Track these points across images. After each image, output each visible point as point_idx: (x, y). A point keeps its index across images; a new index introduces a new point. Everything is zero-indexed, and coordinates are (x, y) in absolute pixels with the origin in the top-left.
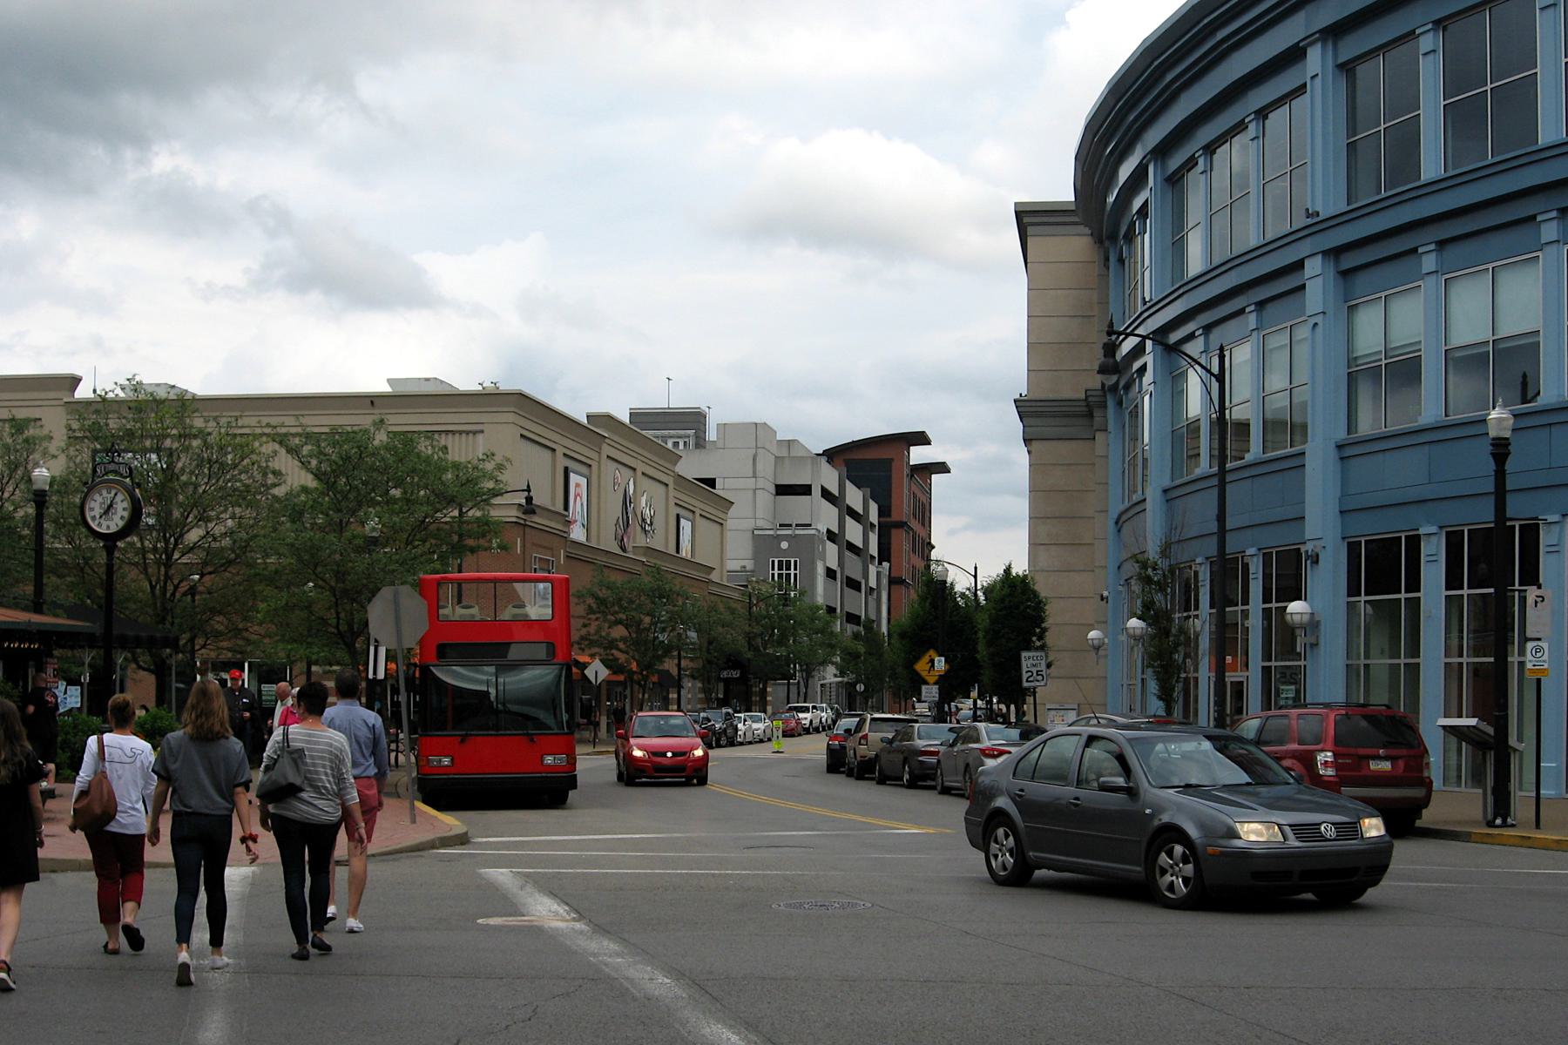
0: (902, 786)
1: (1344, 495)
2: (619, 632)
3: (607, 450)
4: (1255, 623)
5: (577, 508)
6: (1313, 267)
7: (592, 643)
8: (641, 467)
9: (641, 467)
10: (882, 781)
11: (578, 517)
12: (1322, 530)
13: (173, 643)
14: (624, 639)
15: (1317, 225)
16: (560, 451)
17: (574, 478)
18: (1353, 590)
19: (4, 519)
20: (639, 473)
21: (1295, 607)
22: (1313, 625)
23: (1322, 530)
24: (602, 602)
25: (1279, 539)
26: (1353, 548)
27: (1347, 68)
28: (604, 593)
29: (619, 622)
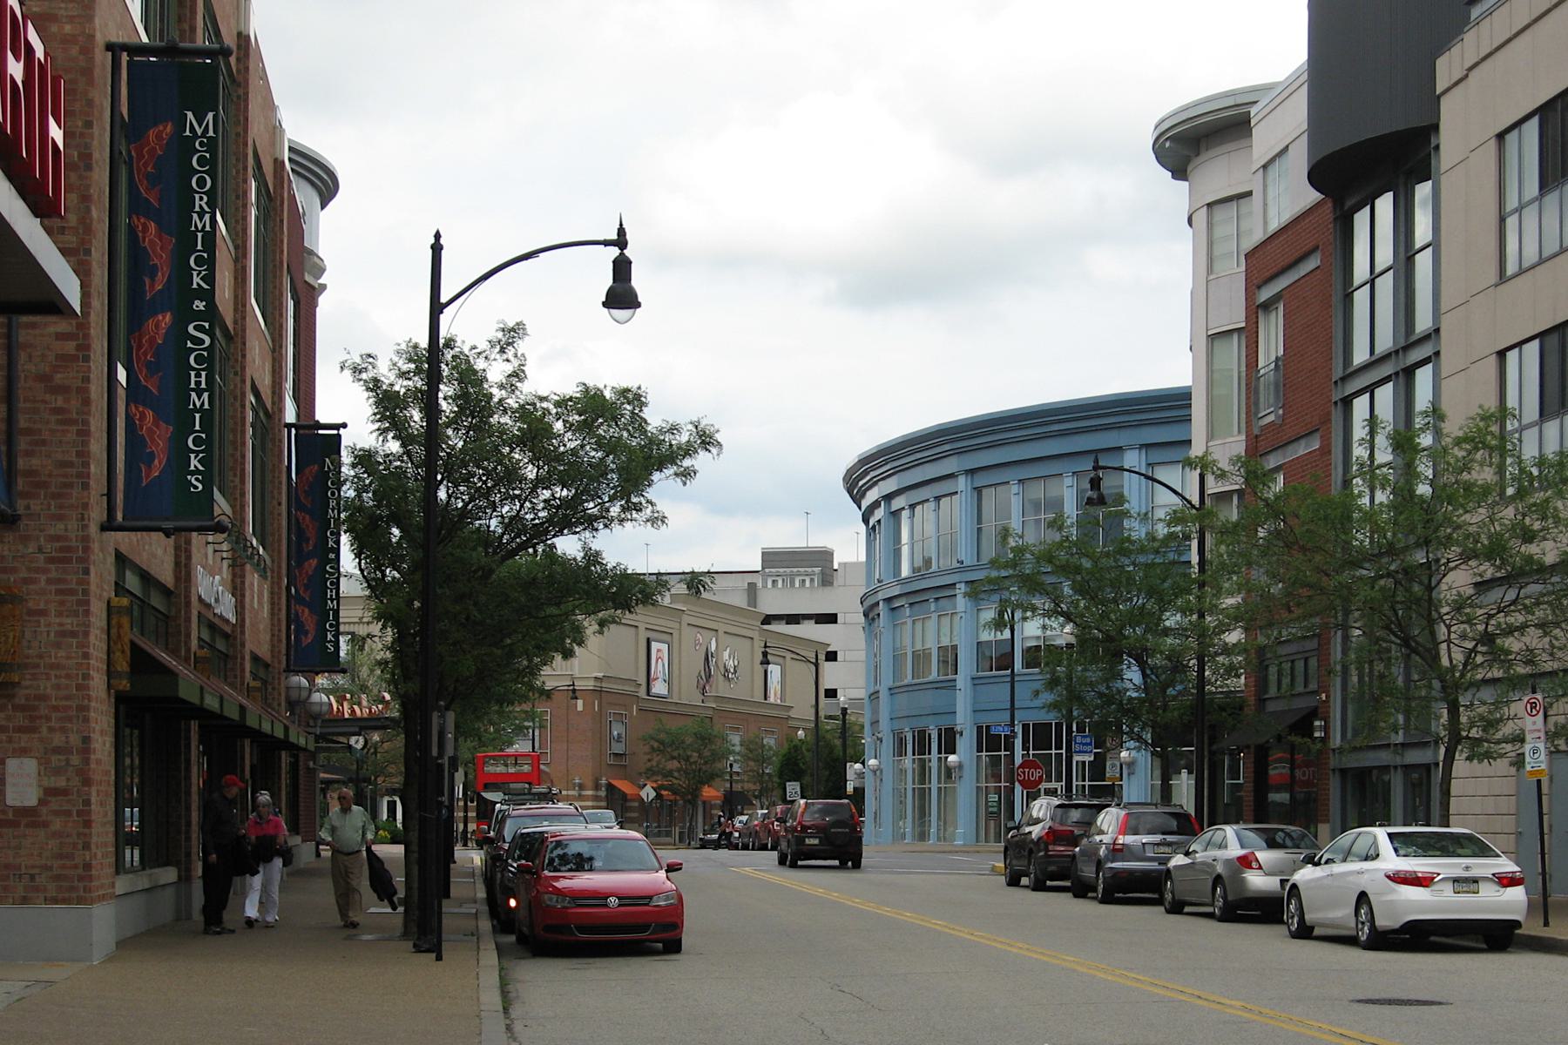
0: (1210, 916)
1: (975, 703)
2: (675, 764)
3: (686, 619)
4: (934, 764)
5: (659, 668)
6: (962, 588)
7: (654, 773)
8: (722, 628)
9: (722, 628)
10: (1177, 908)
11: (660, 675)
12: (963, 719)
13: (368, 781)
14: (679, 770)
15: (962, 568)
16: (642, 627)
17: (655, 646)
18: (979, 750)
19: (4, 570)
20: (721, 633)
21: (952, 758)
22: (960, 766)
23: (963, 719)
24: (662, 743)
25: (945, 722)
26: (979, 729)
27: (978, 490)
28: (662, 736)
29: (673, 758)
